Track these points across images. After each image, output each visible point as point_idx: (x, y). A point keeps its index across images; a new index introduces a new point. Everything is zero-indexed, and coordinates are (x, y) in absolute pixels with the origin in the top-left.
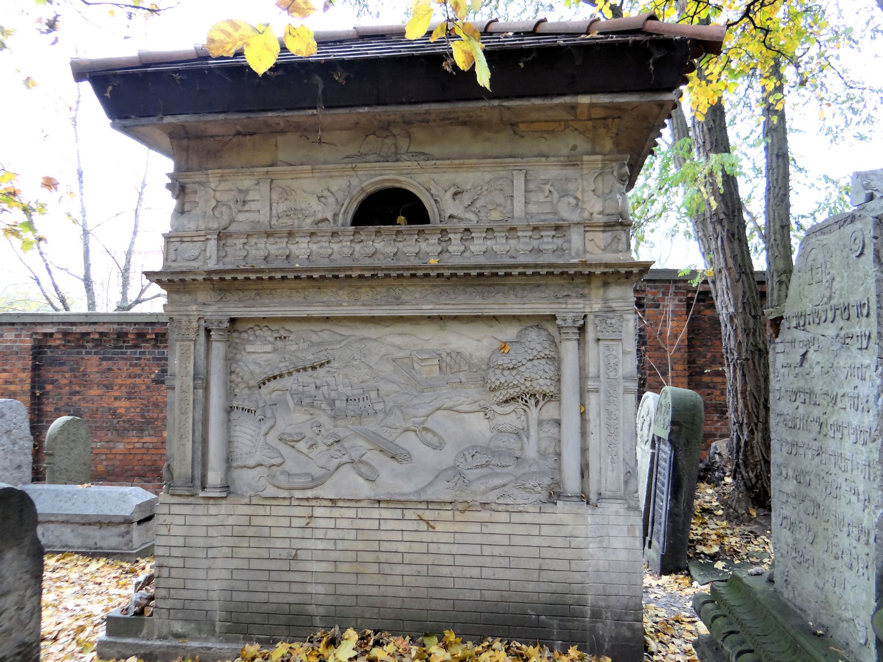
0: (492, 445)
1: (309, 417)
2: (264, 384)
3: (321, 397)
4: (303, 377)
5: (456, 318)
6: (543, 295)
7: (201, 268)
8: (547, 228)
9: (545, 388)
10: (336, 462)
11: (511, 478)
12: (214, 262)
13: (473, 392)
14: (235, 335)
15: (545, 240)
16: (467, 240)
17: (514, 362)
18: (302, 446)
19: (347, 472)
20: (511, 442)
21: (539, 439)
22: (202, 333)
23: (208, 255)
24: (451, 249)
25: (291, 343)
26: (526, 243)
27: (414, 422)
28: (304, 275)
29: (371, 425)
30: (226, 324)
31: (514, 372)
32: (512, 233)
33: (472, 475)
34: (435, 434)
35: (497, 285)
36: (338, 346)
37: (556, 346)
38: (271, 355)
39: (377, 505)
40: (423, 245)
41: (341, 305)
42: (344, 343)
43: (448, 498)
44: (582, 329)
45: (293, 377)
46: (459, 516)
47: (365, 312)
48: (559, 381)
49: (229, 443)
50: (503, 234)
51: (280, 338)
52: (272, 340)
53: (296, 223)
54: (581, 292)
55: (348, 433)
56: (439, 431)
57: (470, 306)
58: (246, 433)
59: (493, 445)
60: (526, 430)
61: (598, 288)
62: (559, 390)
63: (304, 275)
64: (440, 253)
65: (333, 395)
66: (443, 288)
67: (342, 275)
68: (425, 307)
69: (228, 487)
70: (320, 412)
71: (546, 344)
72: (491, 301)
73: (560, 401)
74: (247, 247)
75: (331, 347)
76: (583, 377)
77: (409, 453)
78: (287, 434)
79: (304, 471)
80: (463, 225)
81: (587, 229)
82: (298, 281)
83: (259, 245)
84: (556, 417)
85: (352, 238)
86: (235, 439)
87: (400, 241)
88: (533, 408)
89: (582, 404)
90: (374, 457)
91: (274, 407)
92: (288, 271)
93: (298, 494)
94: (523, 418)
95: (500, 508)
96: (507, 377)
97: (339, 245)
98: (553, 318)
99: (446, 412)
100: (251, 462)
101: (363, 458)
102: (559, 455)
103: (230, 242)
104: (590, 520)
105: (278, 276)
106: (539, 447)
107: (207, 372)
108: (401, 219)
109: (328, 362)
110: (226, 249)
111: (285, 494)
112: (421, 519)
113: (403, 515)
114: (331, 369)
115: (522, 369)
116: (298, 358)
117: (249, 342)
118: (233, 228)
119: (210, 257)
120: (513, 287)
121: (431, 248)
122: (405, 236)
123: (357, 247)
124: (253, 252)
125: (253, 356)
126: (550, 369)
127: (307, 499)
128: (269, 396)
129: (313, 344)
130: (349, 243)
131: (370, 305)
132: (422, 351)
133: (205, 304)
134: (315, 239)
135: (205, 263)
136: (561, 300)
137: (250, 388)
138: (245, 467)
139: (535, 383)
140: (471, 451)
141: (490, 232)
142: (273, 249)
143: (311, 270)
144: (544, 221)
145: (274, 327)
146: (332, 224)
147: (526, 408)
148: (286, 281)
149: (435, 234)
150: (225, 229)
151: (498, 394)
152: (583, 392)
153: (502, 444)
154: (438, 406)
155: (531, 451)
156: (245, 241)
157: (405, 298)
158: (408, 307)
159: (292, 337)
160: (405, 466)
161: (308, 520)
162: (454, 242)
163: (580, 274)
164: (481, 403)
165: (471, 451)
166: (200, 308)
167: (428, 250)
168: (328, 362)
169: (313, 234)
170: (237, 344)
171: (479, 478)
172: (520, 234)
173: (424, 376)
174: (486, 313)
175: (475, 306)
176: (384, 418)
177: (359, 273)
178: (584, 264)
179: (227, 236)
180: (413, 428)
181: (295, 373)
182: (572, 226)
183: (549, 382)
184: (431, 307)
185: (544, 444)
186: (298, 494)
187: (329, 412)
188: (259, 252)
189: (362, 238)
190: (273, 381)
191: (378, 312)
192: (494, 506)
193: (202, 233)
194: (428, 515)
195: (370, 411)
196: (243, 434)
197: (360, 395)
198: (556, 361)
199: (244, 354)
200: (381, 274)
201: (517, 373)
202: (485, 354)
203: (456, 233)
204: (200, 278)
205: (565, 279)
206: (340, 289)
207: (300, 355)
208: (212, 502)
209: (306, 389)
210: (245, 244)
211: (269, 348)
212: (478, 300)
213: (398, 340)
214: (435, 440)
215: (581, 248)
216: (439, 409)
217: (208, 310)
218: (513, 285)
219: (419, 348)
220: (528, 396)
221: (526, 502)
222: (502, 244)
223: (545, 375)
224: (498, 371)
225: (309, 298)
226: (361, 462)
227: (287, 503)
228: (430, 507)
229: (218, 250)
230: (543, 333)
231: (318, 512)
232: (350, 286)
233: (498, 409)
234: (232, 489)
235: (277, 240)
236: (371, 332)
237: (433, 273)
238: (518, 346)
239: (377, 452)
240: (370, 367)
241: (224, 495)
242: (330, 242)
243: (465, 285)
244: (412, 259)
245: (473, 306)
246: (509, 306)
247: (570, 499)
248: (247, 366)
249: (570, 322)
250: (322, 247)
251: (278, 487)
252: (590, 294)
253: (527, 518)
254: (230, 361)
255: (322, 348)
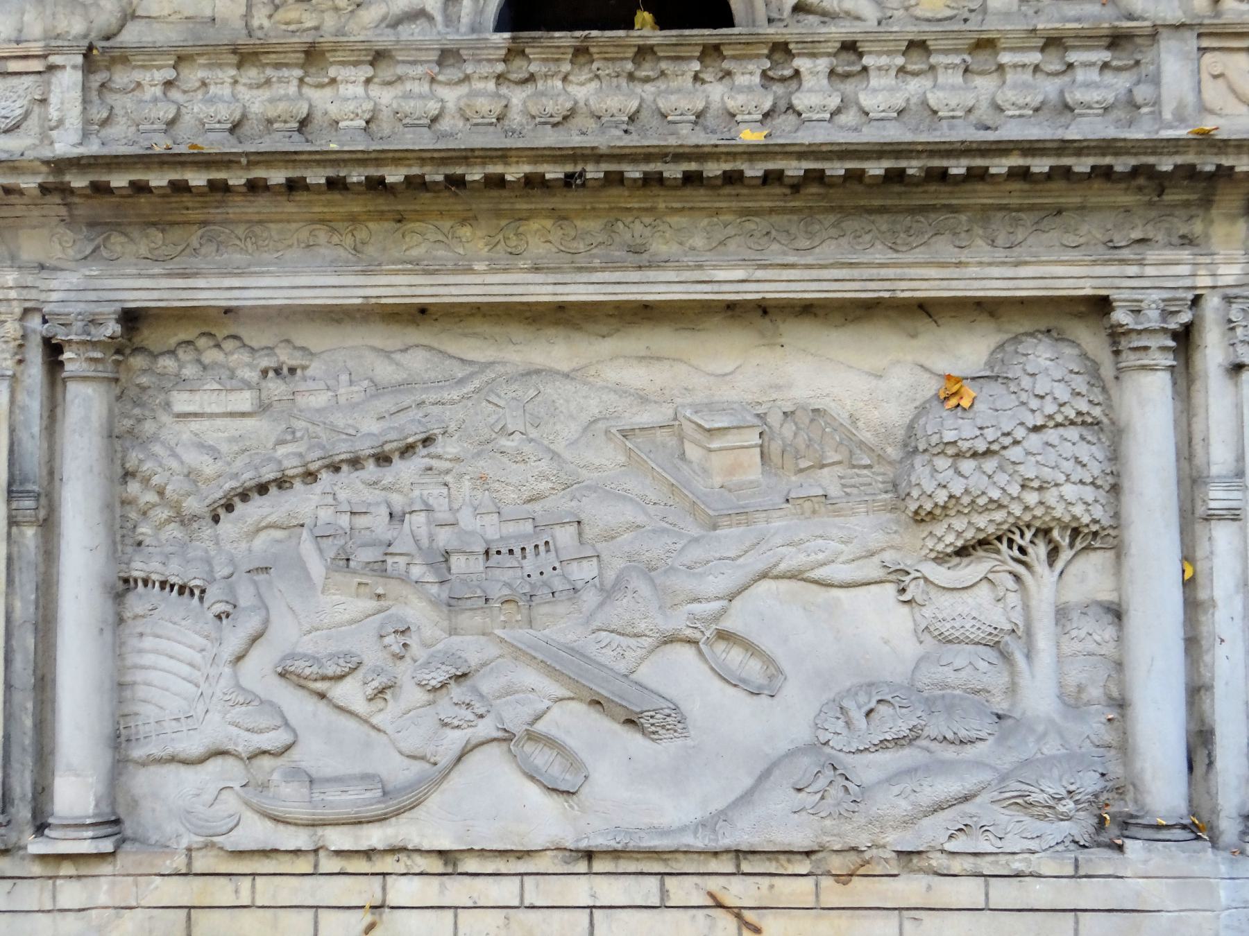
0: (923, 678)
1: (372, 604)
2: (229, 508)
3: (409, 547)
4: (350, 486)
5: (807, 310)
6: (1071, 239)
7: (30, 155)
8: (1087, 39)
9: (1078, 510)
10: (454, 740)
11: (987, 776)
12: (75, 137)
13: (867, 528)
14: (138, 361)
15: (1080, 75)
16: (847, 76)
17: (991, 434)
18: (350, 692)
19: (492, 767)
20: (983, 670)
21: (1060, 659)
22: (36, 356)
23: (54, 114)
24: (800, 101)
25: (311, 385)
26: (1026, 86)
27: (693, 616)
28: (356, 176)
29: (561, 627)
30: (112, 328)
31: (990, 465)
32: (983, 58)
33: (870, 768)
34: (750, 647)
35: (934, 208)
36: (455, 395)
37: (1104, 390)
38: (249, 423)
39: (582, 867)
40: (716, 92)
41: (469, 270)
42: (477, 383)
43: (801, 840)
44: (1185, 339)
45: (318, 488)
46: (833, 893)
47: (541, 290)
48: (1115, 489)
49: (119, 688)
50: (957, 60)
51: (277, 371)
52: (252, 376)
53: (330, 22)
54: (1184, 230)
55: (492, 650)
56: (766, 643)
57: (855, 273)
58: (177, 661)
59: (926, 677)
60: (1027, 636)
61: (1232, 218)
62: (1116, 515)
63: (356, 176)
64: (766, 115)
65: (444, 538)
66: (775, 218)
67: (475, 174)
68: (721, 275)
69: (117, 822)
70: (405, 591)
71: (1080, 383)
72: (919, 255)
73: (1118, 550)
74: (175, 94)
75: (433, 397)
76: (1191, 479)
77: (676, 708)
78: (304, 656)
79: (357, 770)
80: (838, 31)
81: (1206, 43)
82: (336, 196)
83: (213, 89)
84: (1107, 596)
85: (500, 67)
86: (139, 676)
87: (647, 80)
88: (1041, 567)
89: (1188, 557)
90: (573, 723)
91: (261, 577)
92: (308, 163)
93: (338, 839)
94: (1013, 599)
95: (957, 865)
96: (973, 478)
97: (463, 89)
98: (1101, 305)
99: (784, 585)
100: (193, 746)
101: (540, 727)
102: (1121, 704)
103: (121, 77)
104: (1224, 893)
105: (277, 177)
106: (1061, 685)
107: (51, 473)
108: (644, 17)
109: (427, 441)
110: (111, 98)
111: (301, 839)
112: (720, 906)
113: (664, 892)
114: (434, 463)
115: (1015, 453)
116: (334, 430)
117: (180, 382)
118: (131, 36)
119: (61, 122)
120: (985, 213)
121: (741, 99)
122: (663, 65)
123: (518, 97)
124: (197, 108)
125: (195, 425)
126: (1092, 454)
127: (369, 854)
128: (244, 545)
129: (378, 389)
130: (491, 85)
131: (557, 270)
132: (710, 407)
133: (42, 267)
134: (386, 72)
135: (45, 136)
136: (1126, 254)
137: (185, 521)
138: (172, 759)
139: (1051, 497)
140: (862, 698)
141: (916, 55)
142: (258, 103)
143: (380, 158)
144: (1078, 20)
145: (255, 337)
146: (440, 27)
147: (1020, 569)
148: (302, 197)
149: (750, 57)
150: (108, 38)
151: (939, 529)
152: (1192, 518)
153: (951, 677)
154: (761, 566)
155: (1039, 694)
156: (170, 74)
157: (660, 247)
158: (671, 275)
159: (315, 368)
160: (667, 749)
161: (368, 918)
162: (808, 81)
163: (1189, 173)
164: (889, 556)
165: (862, 698)
166: (29, 280)
167: (732, 104)
168: (427, 441)
169: (379, 57)
170: (144, 389)
171: (891, 780)
172: (1005, 58)
173: (718, 480)
174: (906, 290)
175: (873, 273)
176: (601, 605)
177: (527, 169)
178: (1206, 141)
179: (114, 60)
180: (689, 633)
181: (325, 476)
182: (1164, 33)
183: (1089, 493)
184: (740, 274)
185: (1075, 675)
186: (338, 839)
187: (434, 589)
188: (216, 106)
189: (533, 68)
190: (257, 500)
191: (579, 291)
192: (937, 861)
193: (36, 48)
194: (738, 891)
195: (558, 585)
196: (164, 662)
197: (526, 537)
198: (1108, 431)
199: (165, 418)
200: (594, 172)
201: (1001, 468)
202: (895, 414)
203: (813, 55)
204: (29, 183)
205: (1140, 189)
206: (464, 221)
207: (340, 420)
208: (67, 869)
209: (361, 521)
210: (169, 84)
211: (244, 401)
212: (879, 254)
213: (637, 376)
214: (754, 669)
215: (1190, 98)
216: (764, 576)
217: (53, 284)
218: (985, 208)
219: (700, 397)
220: (1029, 535)
221: (1033, 845)
222: (953, 88)
223: (1078, 474)
224: (942, 463)
225: (371, 250)
226: (532, 737)
227: (304, 865)
228: (746, 867)
229: (85, 101)
230: (1068, 351)
231: (403, 891)
232: (498, 214)
233: (939, 574)
234: (128, 829)
235: (269, 72)
236: (555, 352)
237: (753, 171)
238: (996, 388)
239: (579, 708)
240: (555, 456)
241: (107, 846)
242: (433, 80)
243: (841, 209)
244: (685, 130)
245: (867, 273)
246: (973, 271)
247: (1164, 834)
248: (174, 455)
249: (1152, 318)
250: (408, 96)
251: (276, 820)
252: (1207, 236)
253: (1039, 893)
254: (120, 439)
255: (407, 400)
